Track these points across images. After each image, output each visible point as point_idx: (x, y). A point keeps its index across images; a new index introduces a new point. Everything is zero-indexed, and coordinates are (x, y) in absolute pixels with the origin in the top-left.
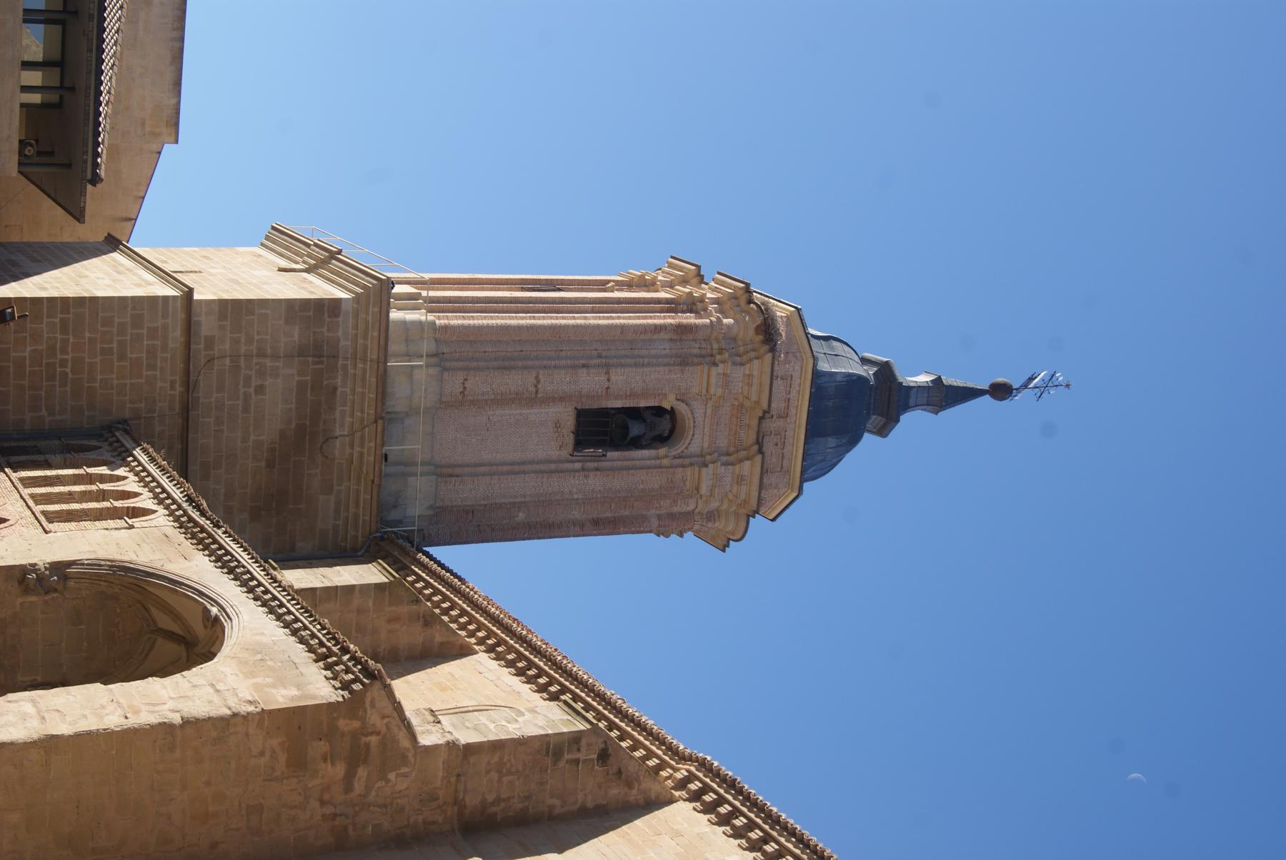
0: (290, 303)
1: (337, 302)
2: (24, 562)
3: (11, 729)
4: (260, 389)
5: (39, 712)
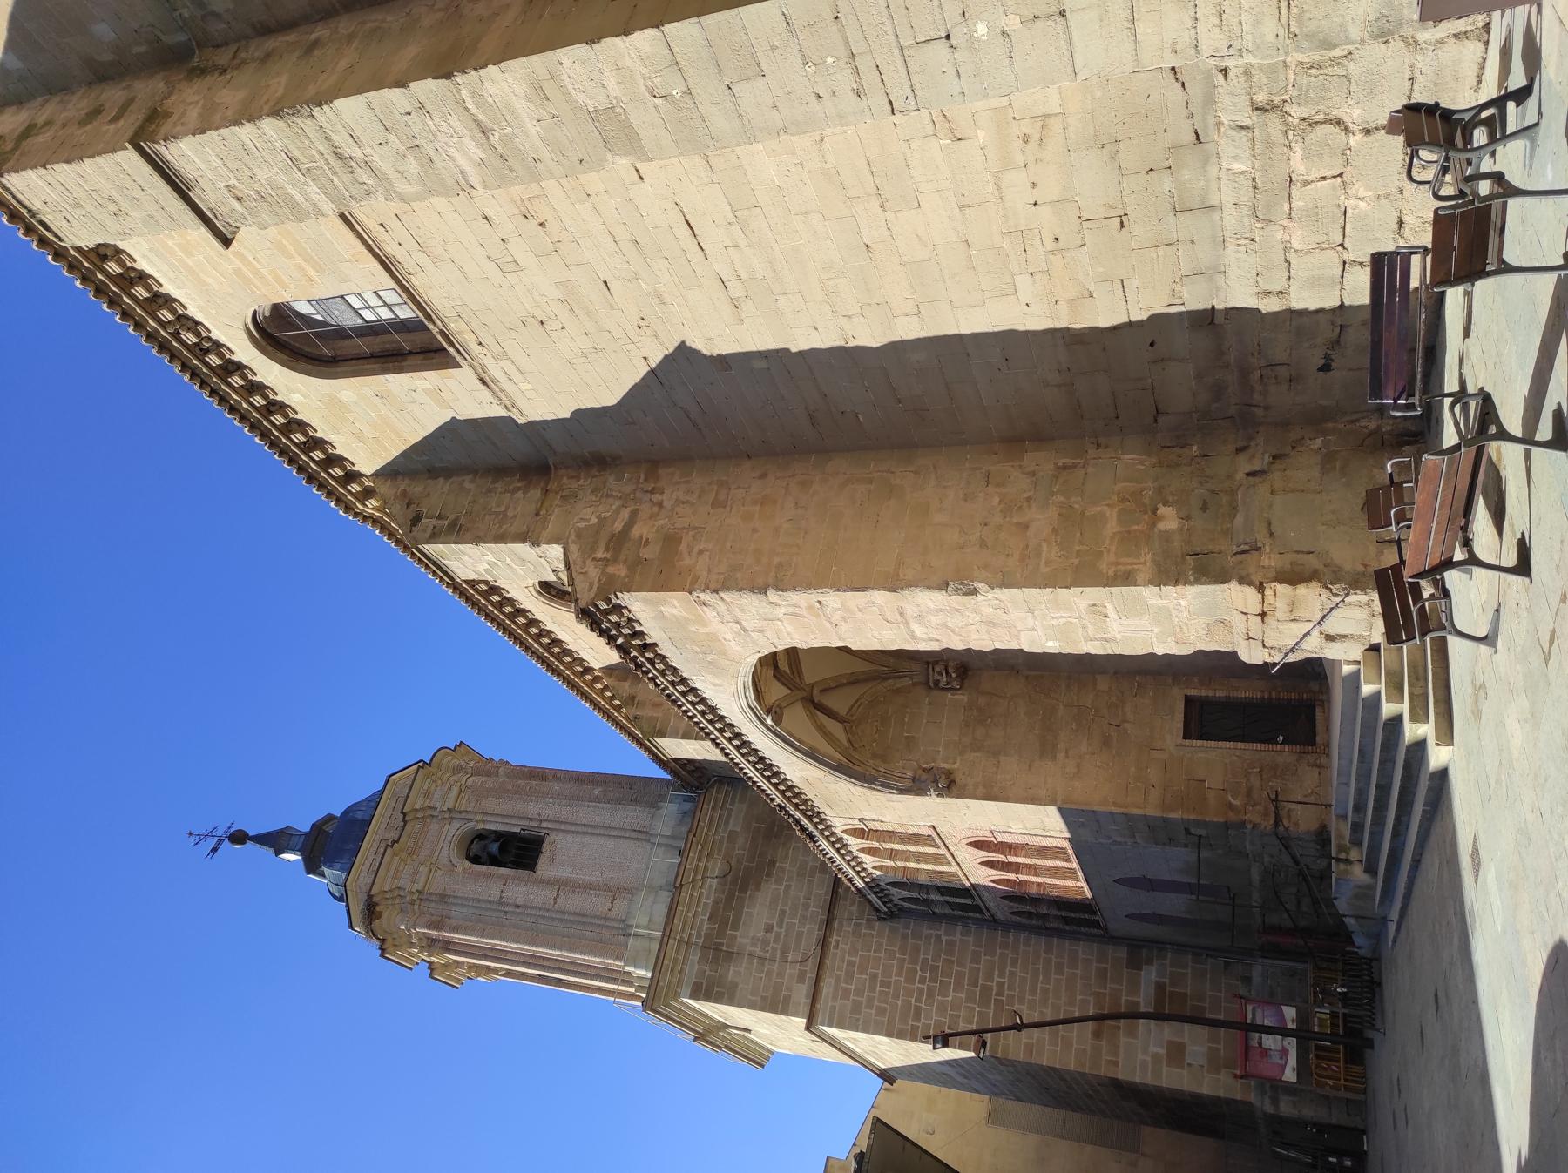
0: (731, 1003)
1: (693, 996)
2: (948, 800)
3: (931, 605)
4: (769, 929)
5: (907, 623)
